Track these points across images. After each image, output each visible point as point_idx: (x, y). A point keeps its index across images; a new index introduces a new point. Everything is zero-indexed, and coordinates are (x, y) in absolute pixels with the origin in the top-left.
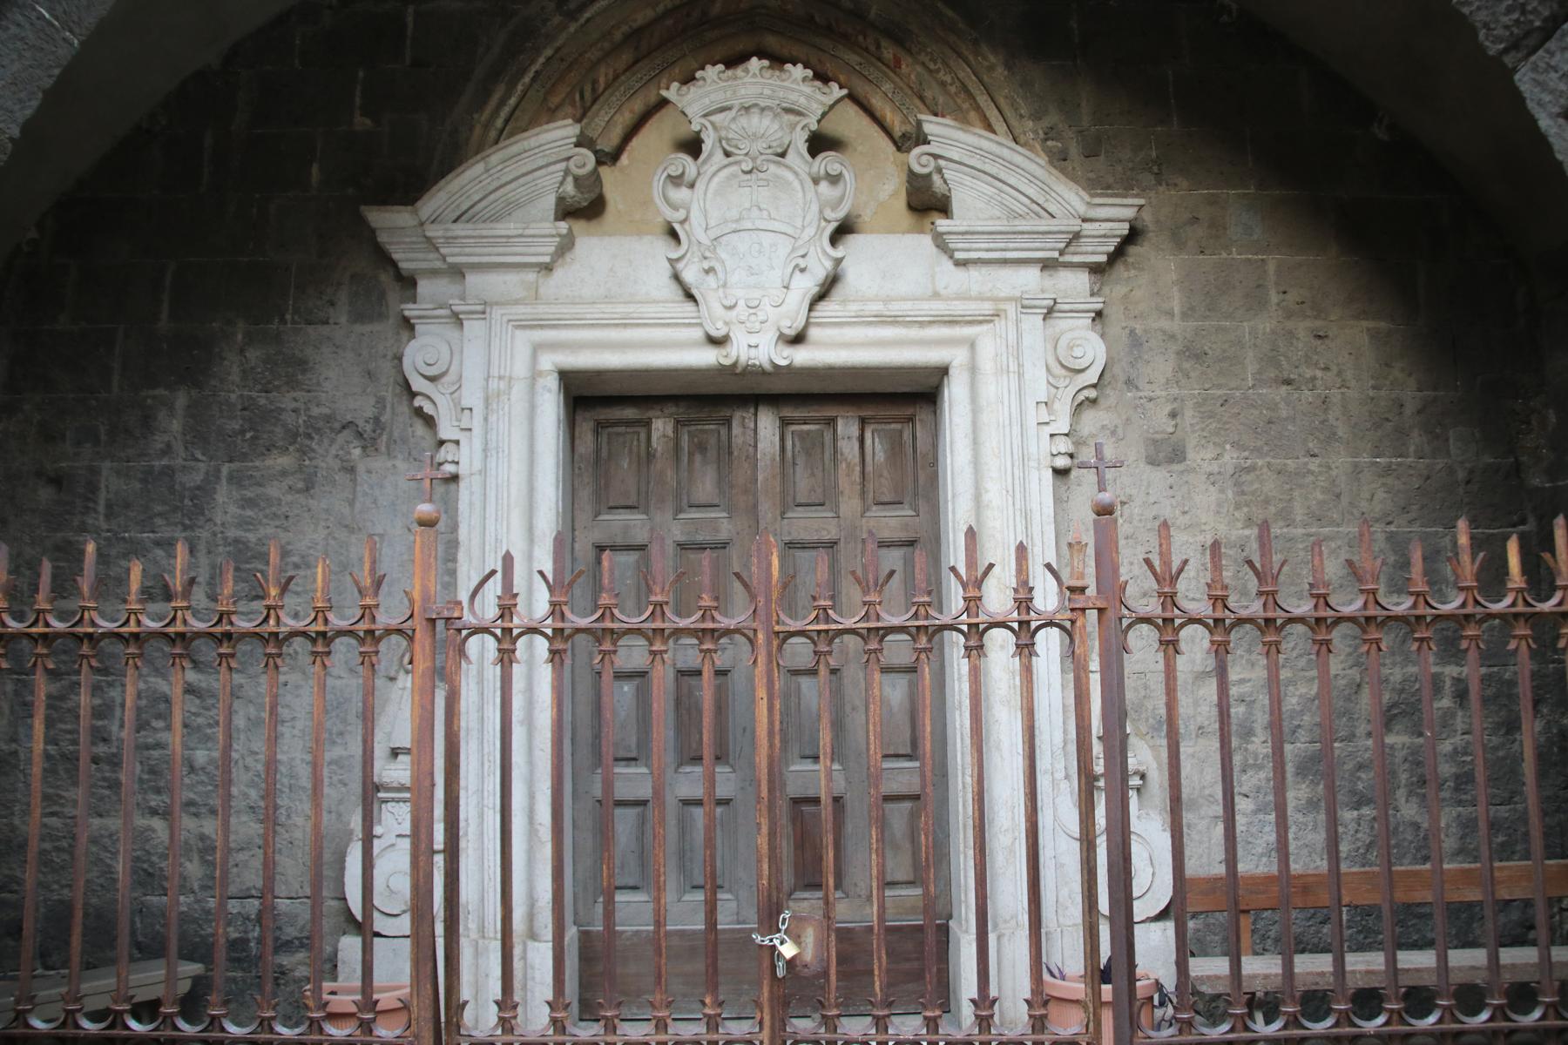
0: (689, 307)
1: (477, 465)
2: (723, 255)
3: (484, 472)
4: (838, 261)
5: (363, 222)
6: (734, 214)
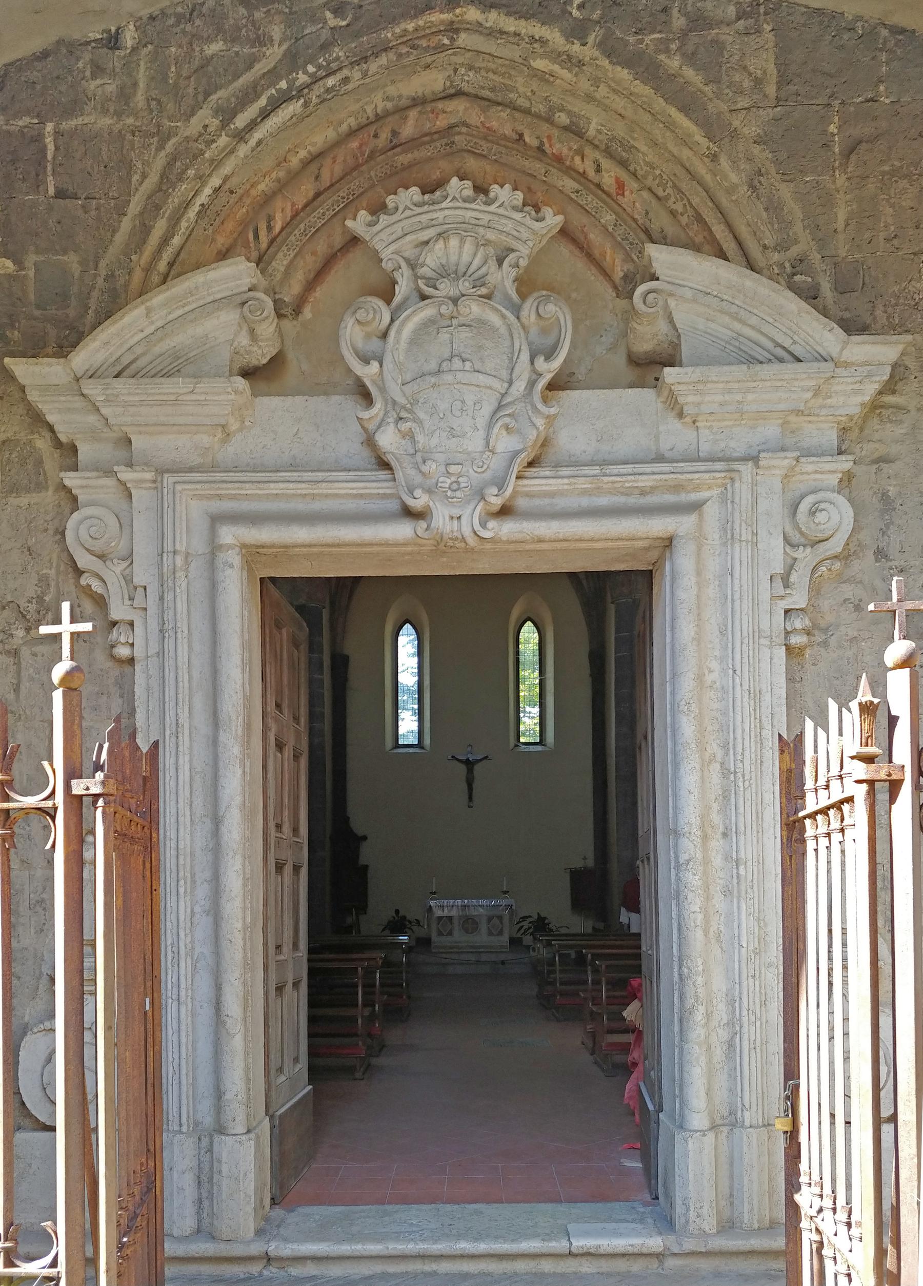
0: (383, 474)
1: (154, 648)
2: (422, 415)
3: (161, 654)
4: (550, 419)
5: (11, 377)
6: (433, 366)
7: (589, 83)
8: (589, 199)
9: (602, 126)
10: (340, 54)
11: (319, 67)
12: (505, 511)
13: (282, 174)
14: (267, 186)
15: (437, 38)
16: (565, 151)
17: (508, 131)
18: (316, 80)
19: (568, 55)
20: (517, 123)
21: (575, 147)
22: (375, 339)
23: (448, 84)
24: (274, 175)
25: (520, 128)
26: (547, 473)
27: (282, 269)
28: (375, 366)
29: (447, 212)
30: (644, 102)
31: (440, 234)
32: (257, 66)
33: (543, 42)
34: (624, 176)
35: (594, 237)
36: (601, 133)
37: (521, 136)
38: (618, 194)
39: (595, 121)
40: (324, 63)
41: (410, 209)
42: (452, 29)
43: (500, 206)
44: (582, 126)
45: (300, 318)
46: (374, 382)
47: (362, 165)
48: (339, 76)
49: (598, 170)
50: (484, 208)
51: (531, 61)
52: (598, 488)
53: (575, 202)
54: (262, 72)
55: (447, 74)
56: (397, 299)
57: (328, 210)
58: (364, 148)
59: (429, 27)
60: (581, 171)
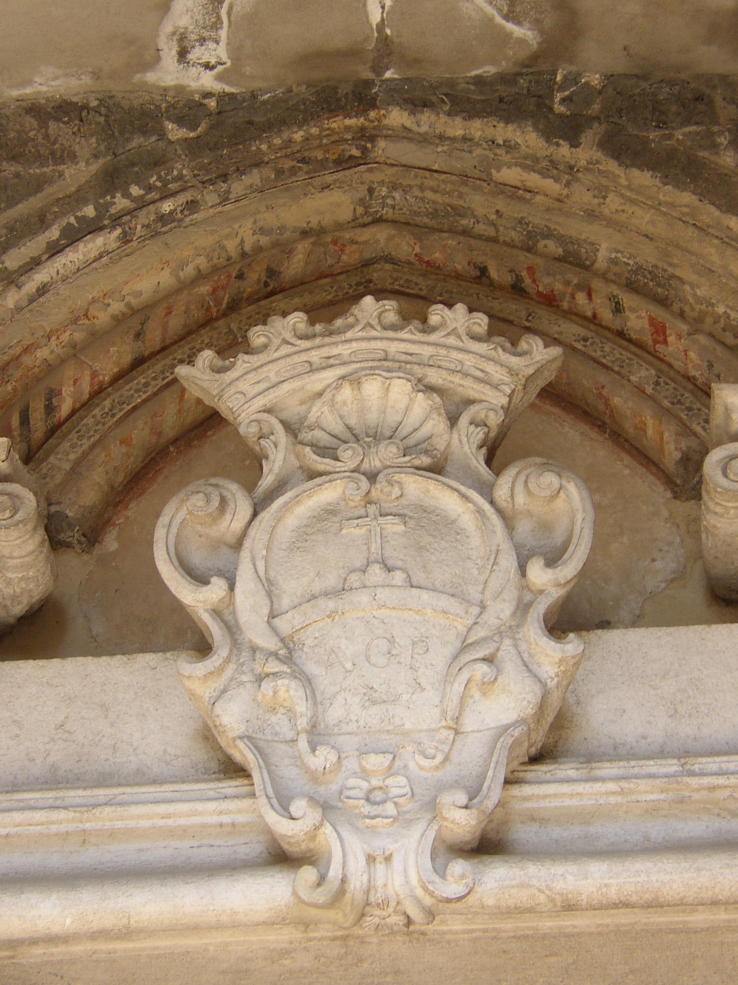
0: (230, 786)
7: (590, 193)
8: (607, 349)
9: (618, 252)
10: (185, 172)
11: (150, 188)
12: (487, 846)
13: (79, 336)
14: (52, 352)
15: (341, 147)
16: (558, 287)
17: (460, 264)
18: (142, 204)
19: (552, 161)
20: (475, 253)
21: (575, 281)
22: (225, 550)
23: (360, 210)
24: (65, 337)
25: (480, 259)
26: (572, 773)
27: (67, 466)
28: (216, 589)
29: (354, 345)
30: (683, 214)
31: (343, 378)
32: (48, 190)
33: (509, 146)
34: (660, 313)
35: (623, 402)
36: (616, 264)
37: (484, 271)
38: (656, 342)
39: (604, 246)
40: (159, 184)
41: (288, 343)
42: (367, 137)
43: (449, 334)
44: (584, 256)
45: (97, 550)
46: (216, 613)
47: (217, 319)
48: (182, 199)
49: (618, 309)
50: (419, 336)
51: (493, 171)
52: (682, 801)
53: (584, 354)
54: (56, 196)
55: (359, 195)
56: (267, 481)
57: (155, 379)
58: (220, 293)
59: (329, 135)
60: (589, 314)
